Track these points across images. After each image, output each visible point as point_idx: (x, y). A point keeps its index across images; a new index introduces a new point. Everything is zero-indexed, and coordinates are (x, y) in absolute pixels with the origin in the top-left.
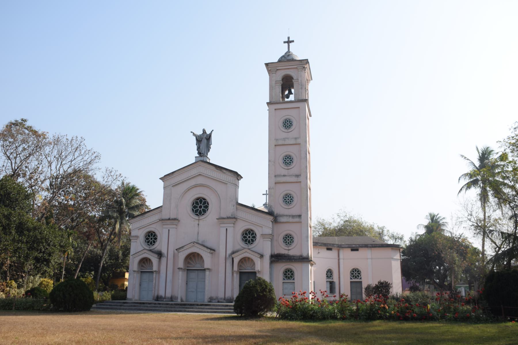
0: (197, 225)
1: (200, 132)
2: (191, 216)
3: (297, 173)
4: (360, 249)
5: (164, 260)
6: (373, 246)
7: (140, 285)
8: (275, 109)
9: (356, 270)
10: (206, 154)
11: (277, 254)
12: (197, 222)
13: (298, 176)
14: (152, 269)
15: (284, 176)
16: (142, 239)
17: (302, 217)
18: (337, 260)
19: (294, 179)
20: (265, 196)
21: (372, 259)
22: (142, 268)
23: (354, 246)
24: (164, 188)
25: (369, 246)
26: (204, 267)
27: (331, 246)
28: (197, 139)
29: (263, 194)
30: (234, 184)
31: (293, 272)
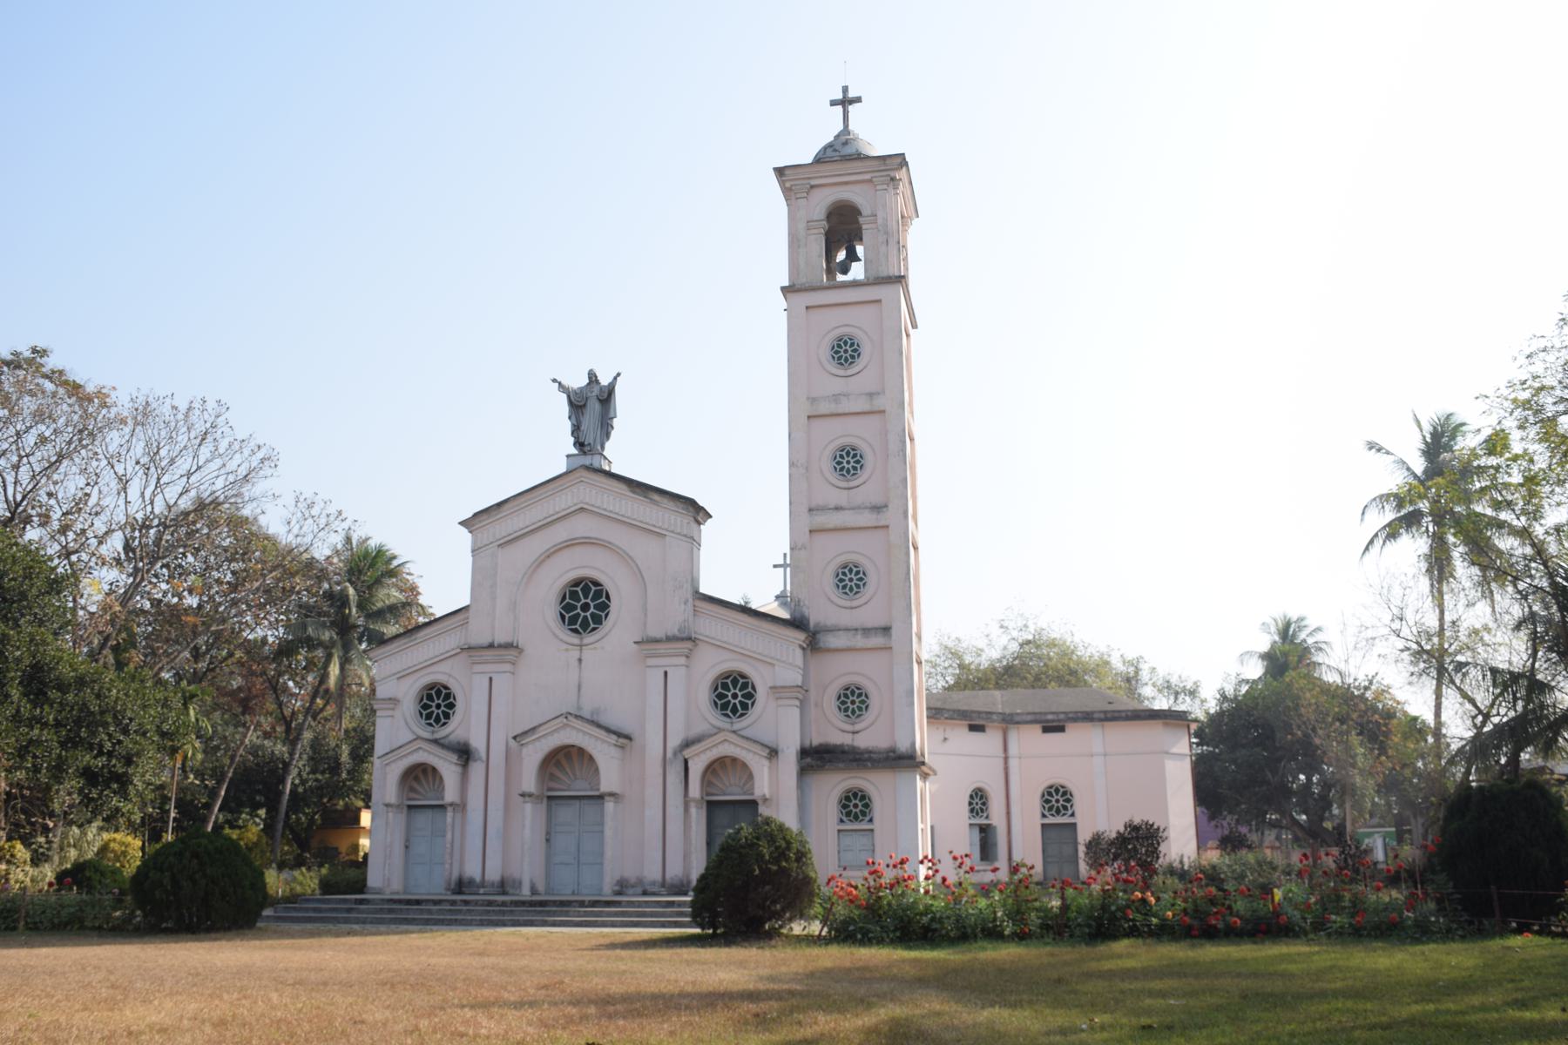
0: (576, 663)
1: (579, 381)
2: (557, 637)
3: (877, 499)
4: (1070, 727)
5: (476, 769)
6: (1109, 715)
7: (407, 847)
8: (807, 308)
9: (1057, 791)
11: (821, 745)
12: (575, 654)
13: (878, 509)
14: (443, 798)
15: (838, 509)
16: (409, 706)
17: (894, 631)
18: (1001, 761)
19: (867, 519)
20: (782, 570)
22: (413, 795)
23: (1050, 717)
25: (1096, 716)
26: (598, 790)
27: (983, 719)
29: (775, 566)
30: (685, 536)
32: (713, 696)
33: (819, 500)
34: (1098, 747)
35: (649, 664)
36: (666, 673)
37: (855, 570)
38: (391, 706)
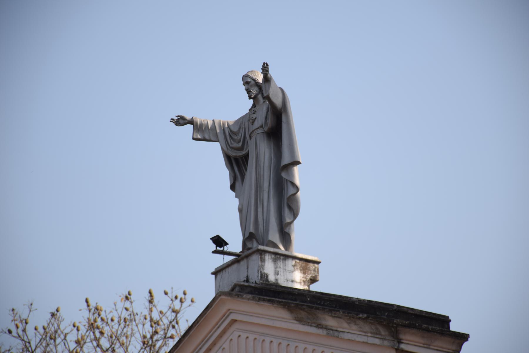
10: (274, 236)
28: (230, 160)
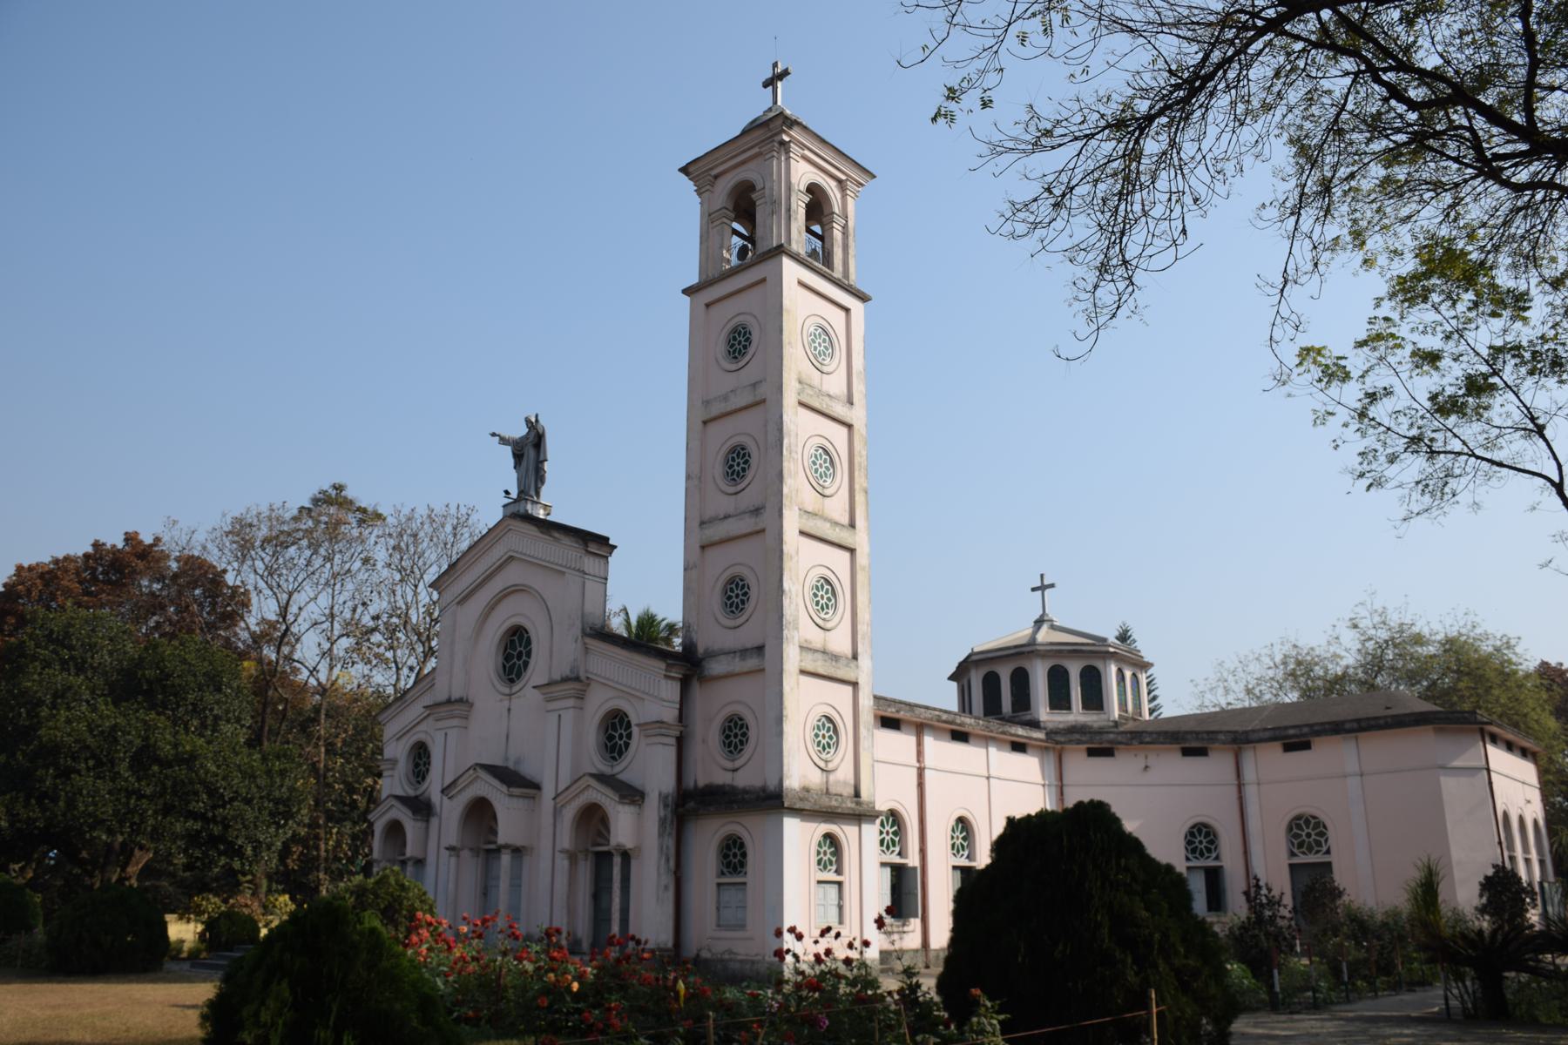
2: (494, 686)
6: (1364, 724)
9: (1307, 822)
10: (532, 492)
12: (506, 703)
13: (757, 511)
14: (404, 854)
15: (726, 517)
16: (403, 766)
17: (767, 648)
18: (1234, 789)
20: (1046, 583)
21: (1362, 775)
23: (1291, 732)
24: (685, 569)
25: (1348, 726)
26: (495, 843)
27: (1203, 739)
29: (1034, 590)
30: (578, 570)
31: (1215, 836)
32: (723, 738)
33: (709, 514)
34: (1352, 765)
35: (549, 709)
36: (560, 716)
37: (741, 583)
38: (390, 766)
